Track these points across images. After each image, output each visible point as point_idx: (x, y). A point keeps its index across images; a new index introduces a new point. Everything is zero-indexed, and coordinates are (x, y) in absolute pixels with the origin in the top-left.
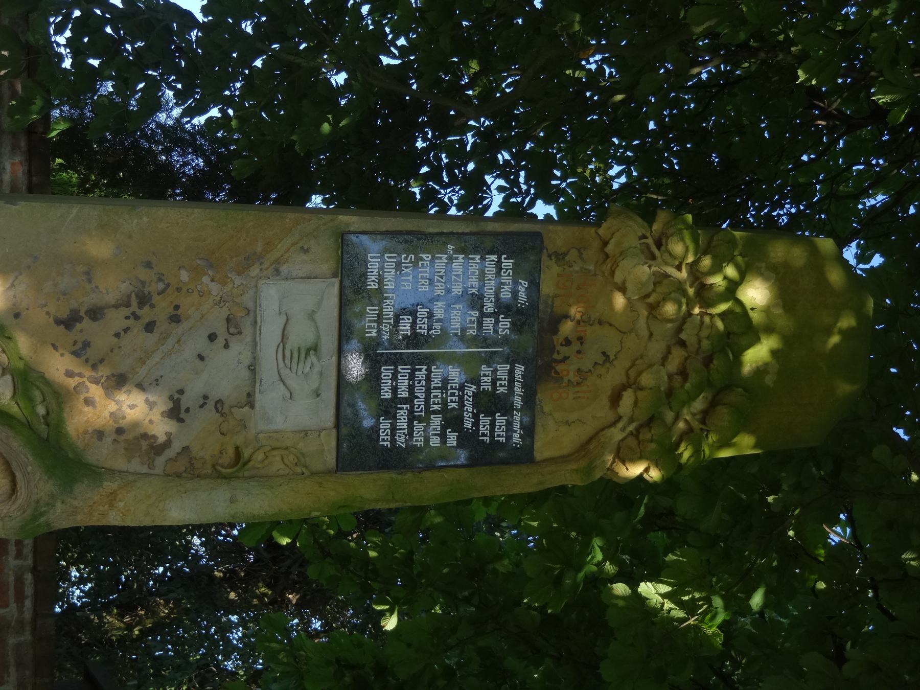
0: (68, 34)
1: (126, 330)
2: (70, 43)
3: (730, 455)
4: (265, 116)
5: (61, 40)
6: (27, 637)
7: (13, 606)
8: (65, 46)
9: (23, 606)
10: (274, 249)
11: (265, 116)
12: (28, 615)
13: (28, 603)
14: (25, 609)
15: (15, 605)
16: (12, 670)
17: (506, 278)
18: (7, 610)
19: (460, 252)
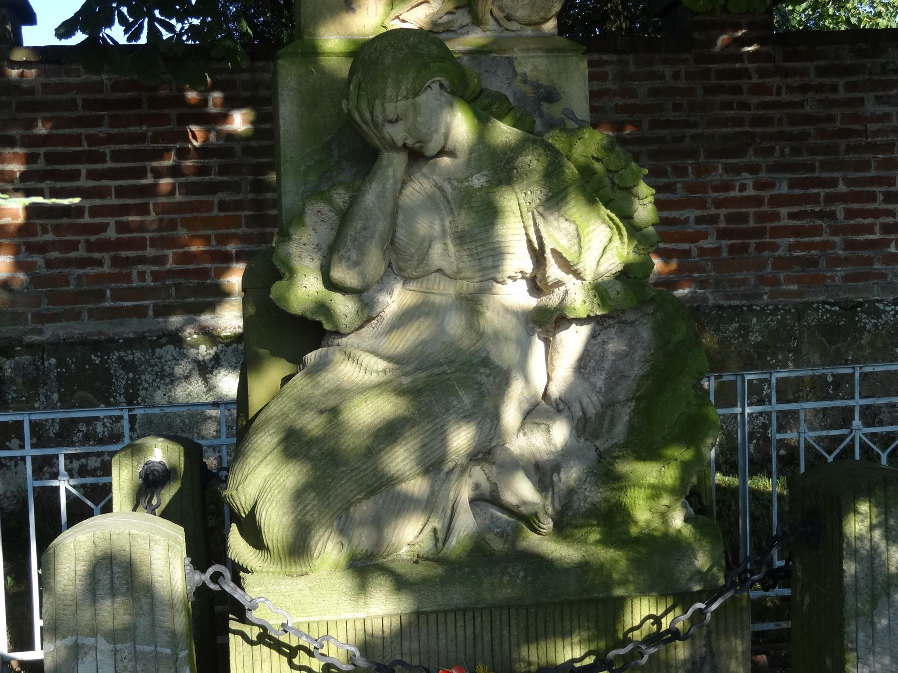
0: (173, 21)
1: (509, 277)
2: (181, 20)
3: (176, 490)
4: (131, 218)
5: (178, 27)
6: (630, 58)
7: (607, 68)
8: (183, 23)
9: (607, 61)
10: (436, 375)
11: (131, 218)
12: (614, 57)
13: (605, 57)
14: (609, 60)
15: (606, 67)
16: (654, 68)
17: (288, 391)
18: (610, 72)
19: (487, 231)
